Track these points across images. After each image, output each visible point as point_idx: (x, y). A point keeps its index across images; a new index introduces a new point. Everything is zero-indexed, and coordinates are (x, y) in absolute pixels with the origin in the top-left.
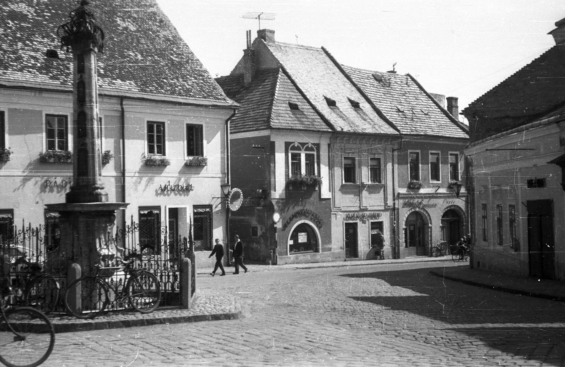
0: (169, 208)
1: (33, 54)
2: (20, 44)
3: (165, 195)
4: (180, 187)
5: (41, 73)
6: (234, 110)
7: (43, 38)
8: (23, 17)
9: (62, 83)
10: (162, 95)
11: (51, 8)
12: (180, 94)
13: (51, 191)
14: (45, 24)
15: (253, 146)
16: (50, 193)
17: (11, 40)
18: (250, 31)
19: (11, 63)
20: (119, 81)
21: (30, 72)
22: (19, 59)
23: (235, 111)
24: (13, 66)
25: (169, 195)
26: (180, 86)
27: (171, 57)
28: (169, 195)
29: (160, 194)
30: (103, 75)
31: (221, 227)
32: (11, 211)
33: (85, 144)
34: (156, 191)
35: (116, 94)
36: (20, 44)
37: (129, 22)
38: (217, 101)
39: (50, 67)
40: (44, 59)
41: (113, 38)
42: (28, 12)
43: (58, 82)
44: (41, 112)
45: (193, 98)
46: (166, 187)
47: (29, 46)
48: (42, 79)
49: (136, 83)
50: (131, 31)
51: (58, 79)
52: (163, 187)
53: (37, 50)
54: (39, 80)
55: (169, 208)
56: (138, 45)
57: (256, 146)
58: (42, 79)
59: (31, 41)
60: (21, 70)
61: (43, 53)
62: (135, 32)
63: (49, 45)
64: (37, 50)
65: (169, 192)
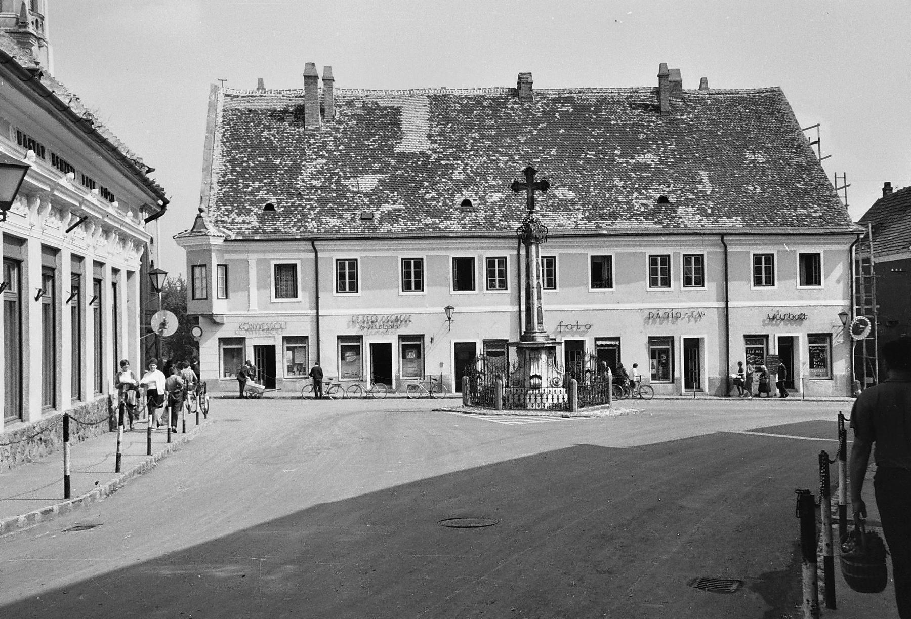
0: (684, 339)
1: (645, 202)
2: (635, 194)
3: (773, 325)
4: (791, 317)
5: (647, 219)
6: (858, 235)
7: (660, 185)
8: (647, 167)
9: (664, 227)
10: (771, 228)
11: (676, 153)
12: (792, 225)
13: (654, 322)
14: (666, 171)
15: (892, 270)
16: (653, 325)
17: (628, 192)
18: (339, 337)
19: (622, 213)
20: (725, 218)
21: (636, 219)
22: (631, 207)
23: (858, 236)
24: (623, 215)
25: (778, 325)
26: (796, 216)
27: (797, 185)
28: (778, 325)
29: (768, 325)
30: (710, 214)
31: (844, 360)
32: (618, 339)
33: (530, 304)
34: (764, 321)
35: (718, 231)
36: (635, 194)
37: (760, 154)
38: (838, 227)
39: (658, 213)
40: (654, 205)
41: (735, 174)
42: (652, 161)
43: (661, 226)
44: (645, 253)
45: (807, 227)
46: (774, 317)
47: (644, 195)
48: (649, 225)
49: (743, 219)
50: (758, 163)
51: (661, 223)
52: (771, 317)
53: (648, 198)
54: (643, 226)
55: (684, 339)
56: (761, 177)
57: (897, 270)
58: (649, 225)
59: (647, 190)
60: (629, 219)
61: (655, 200)
62: (763, 163)
63: (664, 191)
64: (650, 198)
65: (778, 322)
